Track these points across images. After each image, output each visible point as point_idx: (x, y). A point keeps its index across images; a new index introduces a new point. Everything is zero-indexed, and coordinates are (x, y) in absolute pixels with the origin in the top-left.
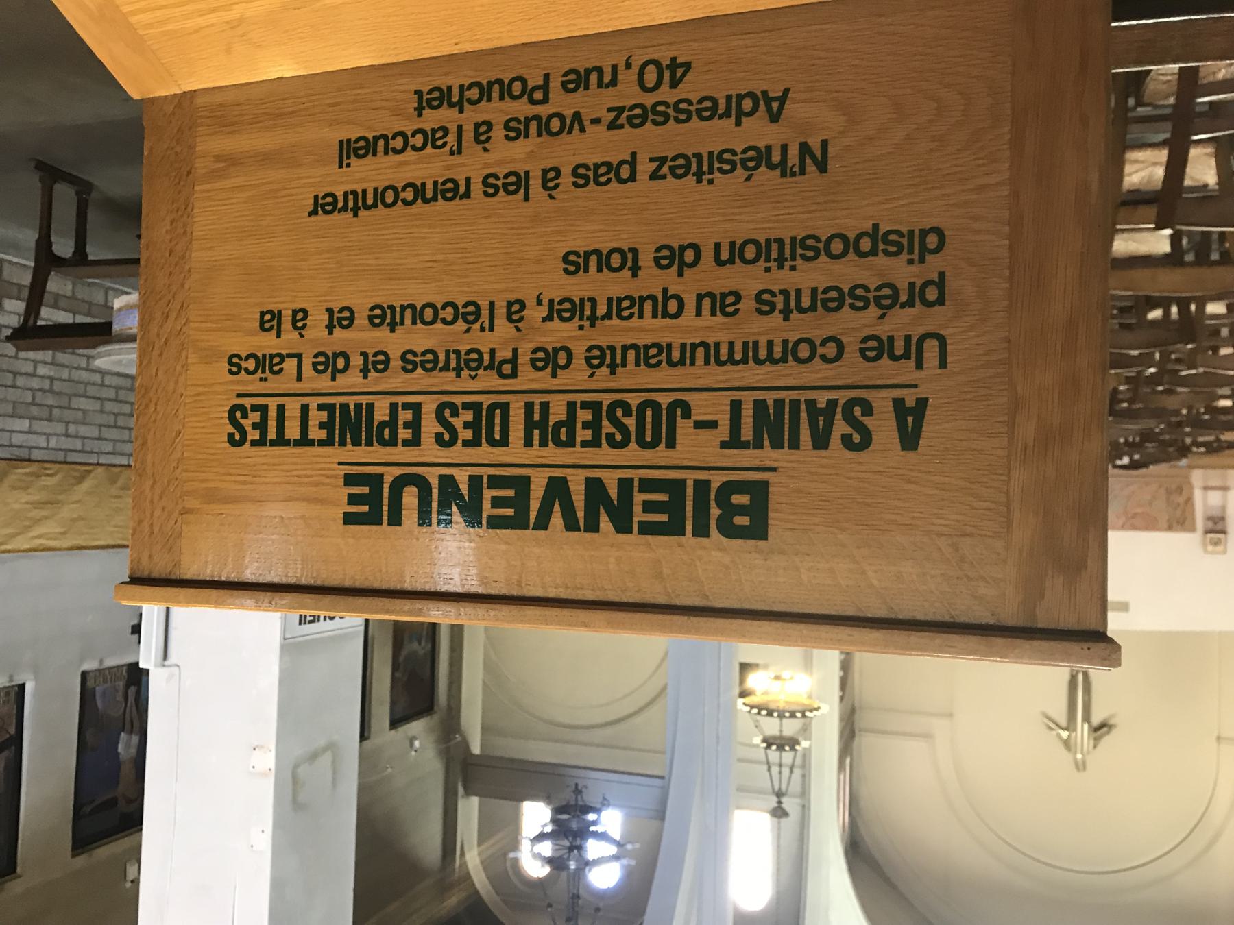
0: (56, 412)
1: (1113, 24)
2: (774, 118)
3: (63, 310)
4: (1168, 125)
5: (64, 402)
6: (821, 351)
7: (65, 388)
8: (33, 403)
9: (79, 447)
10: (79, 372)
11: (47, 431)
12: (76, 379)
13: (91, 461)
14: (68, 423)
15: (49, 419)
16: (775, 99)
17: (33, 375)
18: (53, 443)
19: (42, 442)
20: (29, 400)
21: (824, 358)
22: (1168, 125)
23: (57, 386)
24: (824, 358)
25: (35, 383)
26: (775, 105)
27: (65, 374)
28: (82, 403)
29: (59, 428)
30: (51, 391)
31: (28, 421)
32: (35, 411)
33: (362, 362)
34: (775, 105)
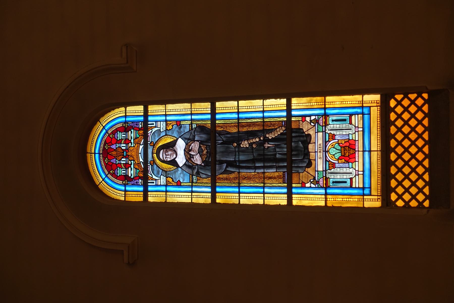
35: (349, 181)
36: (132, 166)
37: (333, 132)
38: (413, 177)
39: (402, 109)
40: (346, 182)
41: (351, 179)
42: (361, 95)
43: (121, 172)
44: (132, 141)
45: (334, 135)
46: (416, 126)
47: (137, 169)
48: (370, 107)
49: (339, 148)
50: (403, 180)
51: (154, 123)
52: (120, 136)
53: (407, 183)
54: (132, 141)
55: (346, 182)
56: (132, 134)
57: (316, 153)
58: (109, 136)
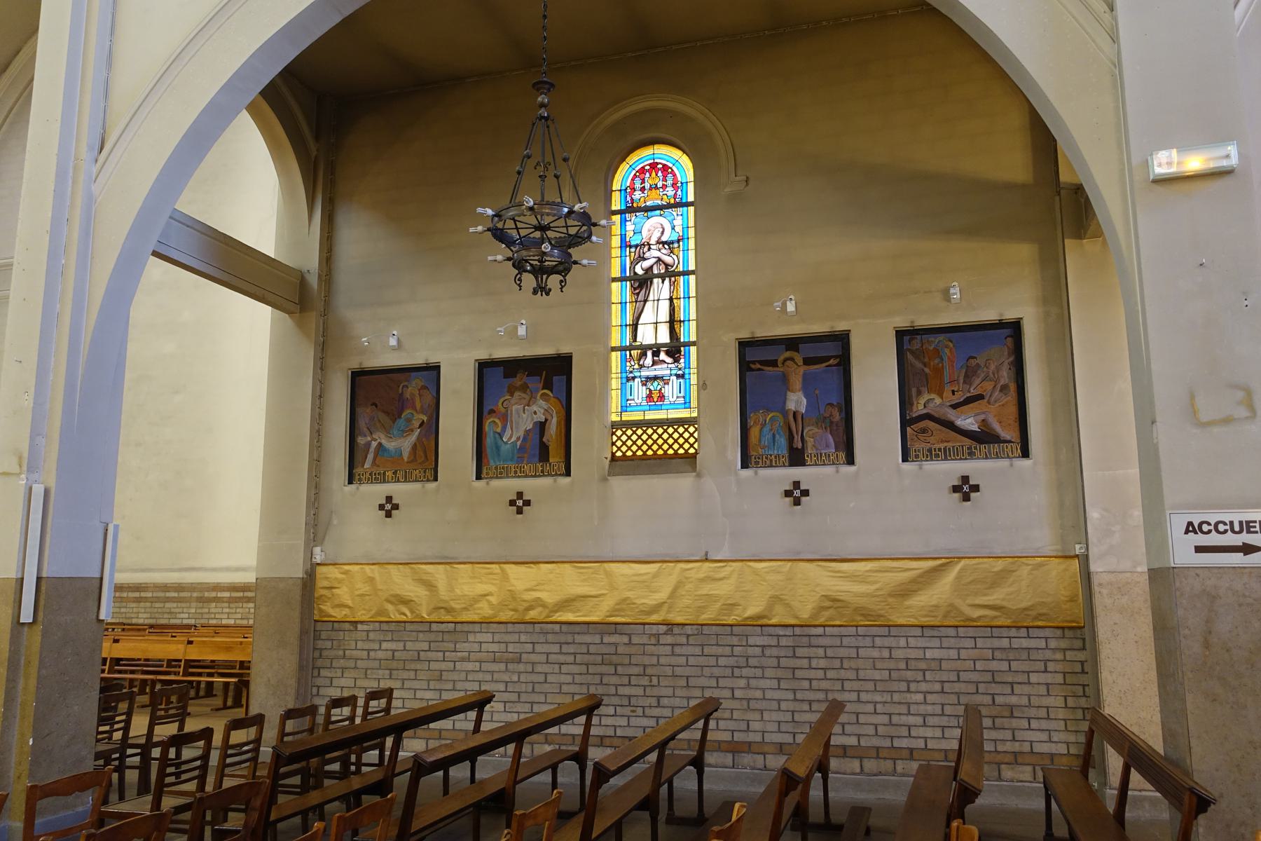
0: (903, 665)
1: (544, 372)
2: (1190, 524)
3: (905, 748)
4: (127, 764)
5: (895, 675)
6: (1212, 527)
7: (895, 686)
8: (924, 671)
9: (877, 639)
10: (884, 700)
11: (909, 650)
12: (885, 694)
13: (831, 628)
14: (890, 658)
15: (907, 660)
16: (1191, 531)
17: (925, 693)
18: (902, 642)
19: (912, 642)
20: (927, 673)
21: (1209, 524)
22: (127, 764)
23: (903, 686)
24: (1209, 524)
25: (924, 687)
26: (1191, 529)
27: (896, 697)
28: (877, 675)
29: (898, 654)
30: (908, 682)
31: (927, 657)
32: (923, 665)
33: (216, 764)
34: (1191, 529)
35: (632, 397)
36: (643, 195)
37: (671, 383)
38: (681, 441)
39: (686, 438)
40: (631, 395)
41: (634, 400)
42: (150, 763)
43: (638, 185)
44: (665, 193)
45: (668, 384)
46: (689, 438)
47: (640, 200)
48: (332, 678)
49: (658, 389)
50: (668, 444)
51: (682, 394)
52: (670, 182)
53: (681, 441)
54: (665, 193)
55: (631, 395)
56: (670, 191)
57: (624, 305)
58: (670, 168)
